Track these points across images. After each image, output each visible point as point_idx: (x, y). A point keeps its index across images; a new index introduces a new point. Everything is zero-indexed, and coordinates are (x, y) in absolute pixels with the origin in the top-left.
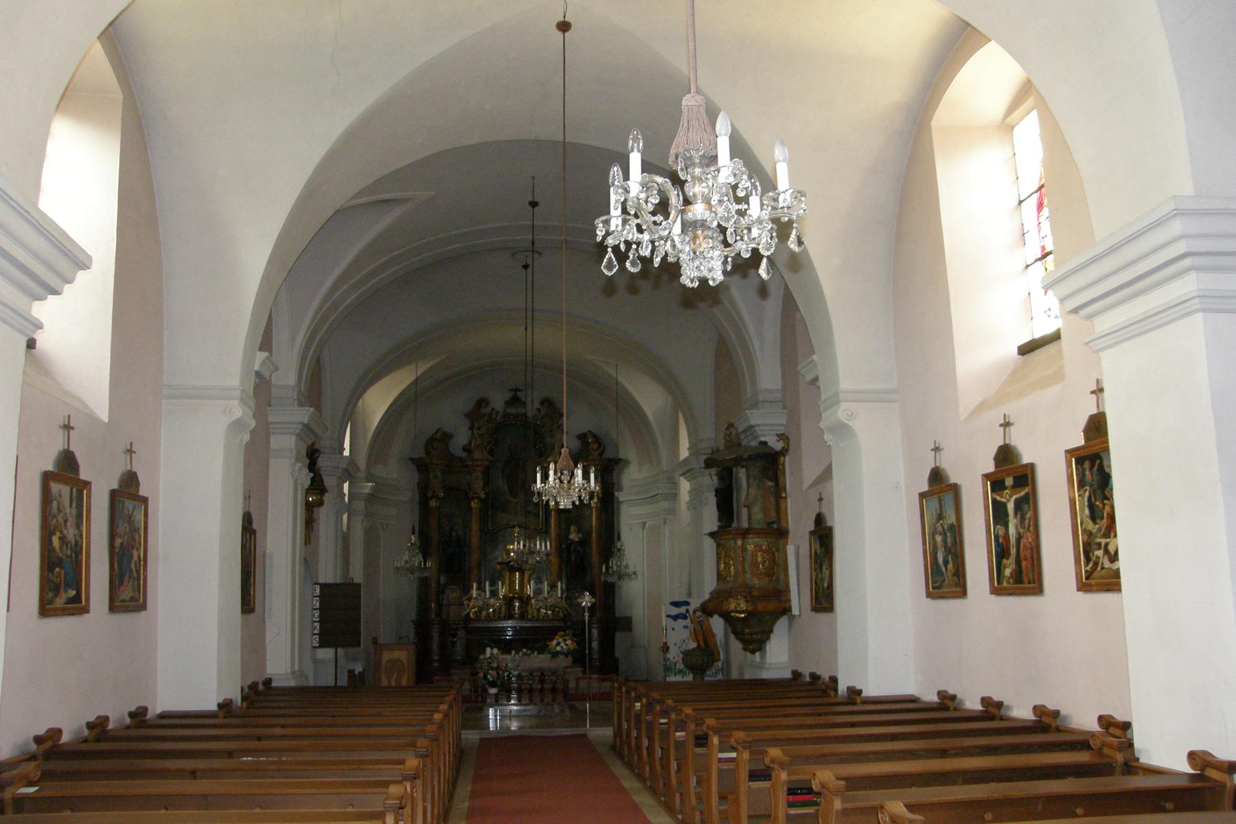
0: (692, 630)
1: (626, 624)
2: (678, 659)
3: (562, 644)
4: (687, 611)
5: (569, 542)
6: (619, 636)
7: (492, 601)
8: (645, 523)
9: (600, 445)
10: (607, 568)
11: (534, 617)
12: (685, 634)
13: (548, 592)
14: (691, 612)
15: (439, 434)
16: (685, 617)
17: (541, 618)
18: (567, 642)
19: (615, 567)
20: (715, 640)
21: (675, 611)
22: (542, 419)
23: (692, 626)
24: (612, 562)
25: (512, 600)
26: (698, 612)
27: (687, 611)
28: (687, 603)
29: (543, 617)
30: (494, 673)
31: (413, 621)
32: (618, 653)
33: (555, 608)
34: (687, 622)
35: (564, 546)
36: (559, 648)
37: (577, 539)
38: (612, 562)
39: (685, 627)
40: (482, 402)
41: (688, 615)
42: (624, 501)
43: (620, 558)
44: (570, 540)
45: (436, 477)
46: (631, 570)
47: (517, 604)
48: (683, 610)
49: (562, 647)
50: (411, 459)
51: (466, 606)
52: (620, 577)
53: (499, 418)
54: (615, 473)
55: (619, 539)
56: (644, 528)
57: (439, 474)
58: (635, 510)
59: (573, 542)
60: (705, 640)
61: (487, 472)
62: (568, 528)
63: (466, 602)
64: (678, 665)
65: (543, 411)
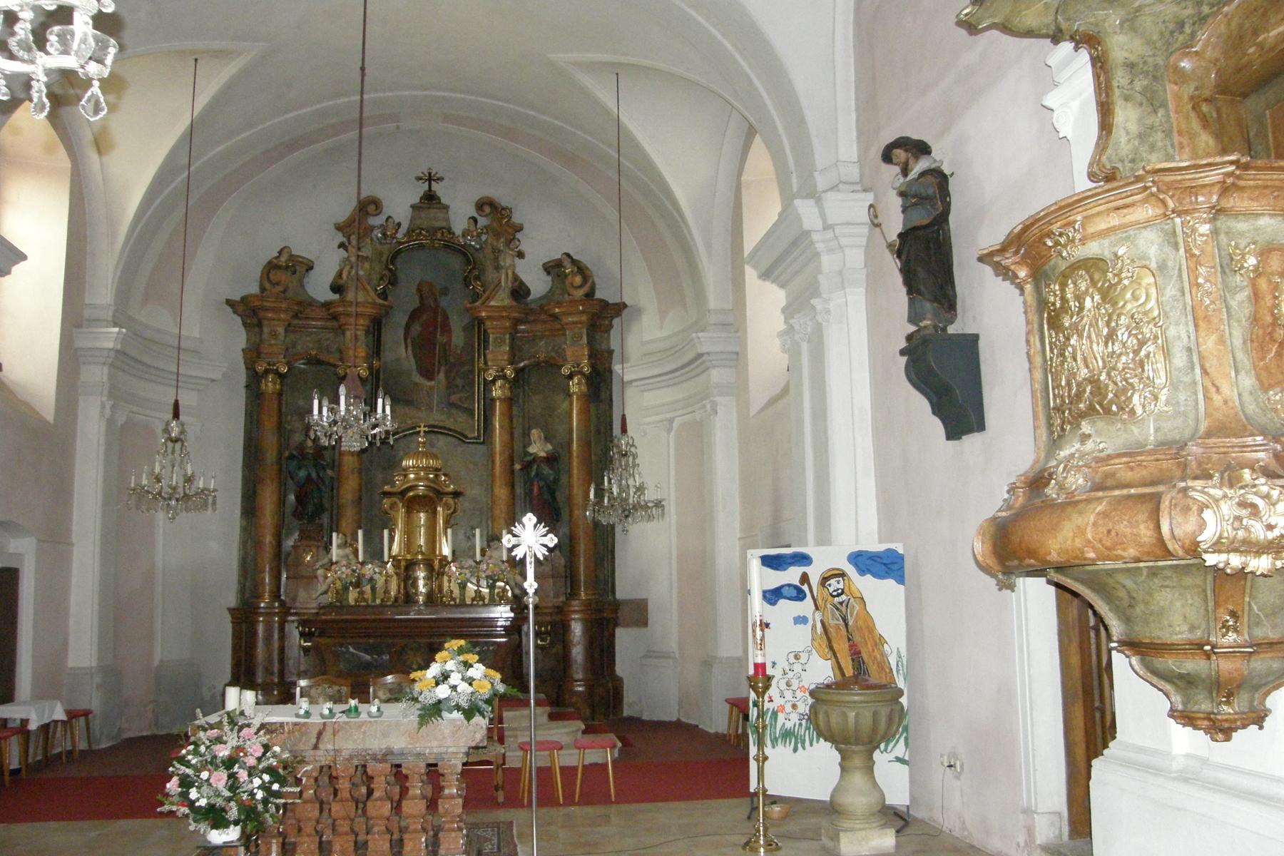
0: (819, 625)
1: (639, 613)
2: (782, 701)
3: (455, 679)
4: (805, 578)
5: (529, 458)
6: (624, 637)
7: (369, 569)
8: (671, 420)
9: (586, 278)
10: (600, 493)
11: (454, 599)
12: (802, 637)
13: (483, 553)
14: (815, 580)
15: (283, 259)
16: (799, 596)
17: (468, 602)
18: (471, 673)
19: (615, 490)
20: (883, 655)
21: (777, 578)
22: (479, 235)
23: (818, 616)
24: (610, 480)
25: (411, 565)
26: (833, 581)
27: (805, 578)
28: (803, 559)
29: (473, 600)
30: (220, 779)
31: (230, 610)
32: (620, 669)
33: (495, 581)
34: (806, 607)
35: (517, 467)
36: (443, 692)
37: (543, 454)
38: (610, 480)
39: (801, 620)
40: (368, 206)
41: (805, 588)
42: (631, 382)
43: (629, 470)
44: (531, 454)
45: (274, 335)
46: (650, 495)
47: (1275, 666)
48: (792, 575)
49: (454, 688)
50: (229, 303)
51: (321, 579)
52: (628, 512)
53: (399, 236)
54: (614, 333)
55: (624, 430)
56: (669, 430)
57: (281, 330)
58: (652, 398)
59: (535, 459)
60: (856, 656)
61: (376, 327)
62: (526, 434)
63: (320, 572)
64: (781, 717)
65: (483, 222)
